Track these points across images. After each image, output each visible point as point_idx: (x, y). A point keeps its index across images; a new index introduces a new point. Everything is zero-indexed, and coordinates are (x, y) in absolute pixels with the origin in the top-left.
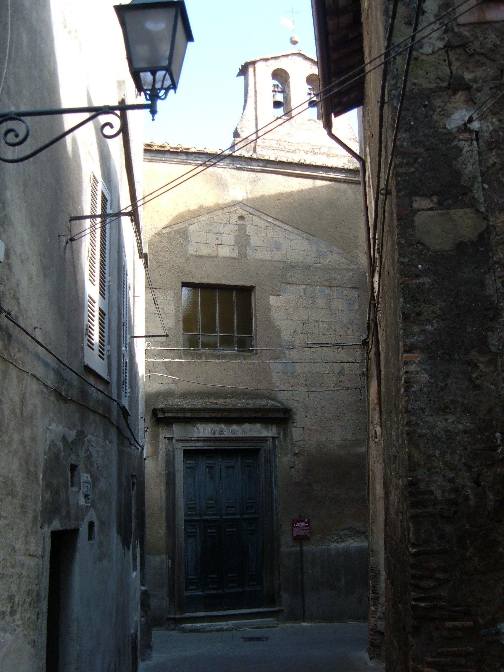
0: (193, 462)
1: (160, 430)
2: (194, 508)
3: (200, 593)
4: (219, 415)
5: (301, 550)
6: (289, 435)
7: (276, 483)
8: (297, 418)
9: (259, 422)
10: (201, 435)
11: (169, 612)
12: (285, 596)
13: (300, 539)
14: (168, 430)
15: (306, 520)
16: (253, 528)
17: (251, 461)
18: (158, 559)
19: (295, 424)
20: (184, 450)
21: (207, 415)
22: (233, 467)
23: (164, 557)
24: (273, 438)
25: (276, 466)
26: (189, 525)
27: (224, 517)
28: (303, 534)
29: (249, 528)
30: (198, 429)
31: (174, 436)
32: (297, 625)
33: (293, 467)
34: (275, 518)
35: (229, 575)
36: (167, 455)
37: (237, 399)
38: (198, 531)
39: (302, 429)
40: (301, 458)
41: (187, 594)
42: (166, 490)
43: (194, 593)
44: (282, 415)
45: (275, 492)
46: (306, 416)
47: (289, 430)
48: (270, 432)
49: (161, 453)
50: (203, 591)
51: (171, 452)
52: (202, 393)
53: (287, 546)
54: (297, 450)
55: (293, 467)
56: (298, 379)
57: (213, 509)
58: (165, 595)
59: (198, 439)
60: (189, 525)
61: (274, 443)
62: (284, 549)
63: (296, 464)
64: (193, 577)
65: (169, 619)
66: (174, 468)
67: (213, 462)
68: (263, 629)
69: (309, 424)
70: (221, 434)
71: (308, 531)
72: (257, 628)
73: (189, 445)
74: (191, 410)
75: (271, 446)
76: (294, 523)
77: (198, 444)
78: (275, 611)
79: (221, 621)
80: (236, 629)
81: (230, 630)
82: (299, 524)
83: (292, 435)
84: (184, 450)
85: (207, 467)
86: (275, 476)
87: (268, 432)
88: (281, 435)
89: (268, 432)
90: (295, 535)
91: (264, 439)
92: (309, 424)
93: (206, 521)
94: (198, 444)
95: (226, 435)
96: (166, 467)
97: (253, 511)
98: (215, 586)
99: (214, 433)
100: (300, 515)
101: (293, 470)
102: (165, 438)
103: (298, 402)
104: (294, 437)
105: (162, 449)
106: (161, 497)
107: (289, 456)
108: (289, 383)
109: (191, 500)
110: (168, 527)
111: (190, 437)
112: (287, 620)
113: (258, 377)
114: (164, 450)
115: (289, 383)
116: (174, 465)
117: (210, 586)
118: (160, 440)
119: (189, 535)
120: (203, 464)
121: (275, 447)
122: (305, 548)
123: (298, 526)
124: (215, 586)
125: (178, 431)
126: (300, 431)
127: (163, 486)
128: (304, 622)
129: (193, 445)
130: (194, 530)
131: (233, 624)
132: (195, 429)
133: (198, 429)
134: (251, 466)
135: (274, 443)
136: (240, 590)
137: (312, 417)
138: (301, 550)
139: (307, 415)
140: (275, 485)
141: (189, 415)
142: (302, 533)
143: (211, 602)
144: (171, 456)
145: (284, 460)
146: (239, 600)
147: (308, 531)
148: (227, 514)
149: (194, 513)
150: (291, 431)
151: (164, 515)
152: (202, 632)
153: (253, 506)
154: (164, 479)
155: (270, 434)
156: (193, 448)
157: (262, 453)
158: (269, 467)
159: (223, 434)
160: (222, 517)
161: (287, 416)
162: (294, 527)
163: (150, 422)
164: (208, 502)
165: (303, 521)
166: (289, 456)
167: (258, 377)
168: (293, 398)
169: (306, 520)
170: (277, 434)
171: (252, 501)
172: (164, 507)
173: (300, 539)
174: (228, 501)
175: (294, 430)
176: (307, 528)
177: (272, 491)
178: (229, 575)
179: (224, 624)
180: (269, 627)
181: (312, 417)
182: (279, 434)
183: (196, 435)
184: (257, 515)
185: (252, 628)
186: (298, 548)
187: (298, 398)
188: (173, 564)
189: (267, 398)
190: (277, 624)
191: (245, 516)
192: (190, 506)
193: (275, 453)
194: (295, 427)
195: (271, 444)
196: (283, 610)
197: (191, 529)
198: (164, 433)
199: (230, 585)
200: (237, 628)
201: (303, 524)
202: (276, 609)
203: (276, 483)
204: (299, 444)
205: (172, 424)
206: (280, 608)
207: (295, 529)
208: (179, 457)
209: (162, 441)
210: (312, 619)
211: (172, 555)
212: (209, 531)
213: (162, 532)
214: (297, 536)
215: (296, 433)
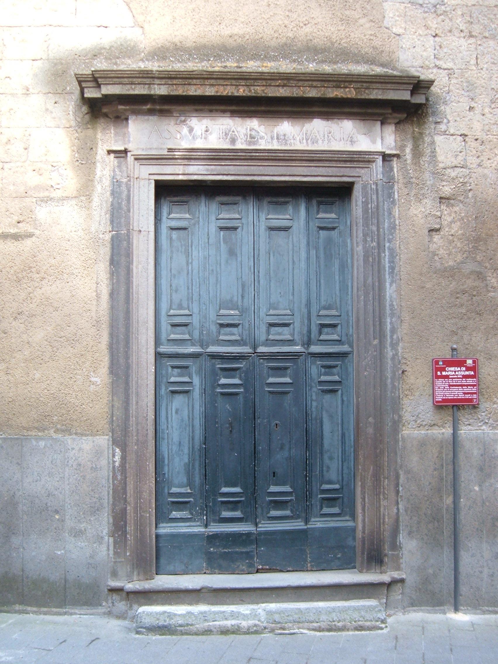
0: (187, 216)
1: (99, 135)
2: (186, 325)
3: (196, 530)
4: (241, 91)
5: (455, 435)
6: (428, 151)
7: (392, 268)
8: (448, 110)
9: (349, 115)
10: (199, 144)
11: (114, 574)
12: (410, 547)
13: (453, 408)
14: (116, 134)
15: (469, 362)
16: (336, 378)
17: (333, 216)
18: (87, 444)
19: (443, 127)
20: (156, 182)
21: (210, 91)
22: (286, 229)
23: (103, 441)
24: (386, 157)
25: (393, 227)
26: (173, 367)
27: (261, 349)
28: (461, 396)
29: (323, 378)
30: (191, 130)
31: (130, 147)
32: (439, 617)
33: (437, 230)
34: (389, 353)
35: (273, 489)
36: (113, 193)
37: (294, 61)
38: (196, 381)
39: (461, 138)
40: (457, 209)
41: (165, 529)
42: (111, 278)
43: (183, 529)
44: (405, 96)
45: (390, 291)
46: (471, 109)
47: (427, 139)
48: (379, 141)
49: (99, 188)
50: (206, 526)
51: (124, 188)
52: (205, 47)
53: (417, 422)
54: (447, 190)
55: (437, 230)
56: (451, 20)
57: (234, 330)
58: (105, 531)
59: (191, 156)
60: (173, 367)
61: (388, 171)
62: (410, 432)
63: (444, 223)
64: (182, 490)
65: (113, 590)
66: (128, 224)
67: (237, 216)
68: (344, 633)
69: (477, 126)
70: (250, 143)
71: (474, 390)
72: (329, 630)
73: (169, 169)
74: (169, 77)
75: (380, 176)
76: (438, 368)
77: (192, 169)
78: (381, 584)
79: (242, 602)
80: (272, 631)
81: (256, 632)
82: (450, 371)
83: (434, 152)
84: (156, 182)
85: (221, 228)
86: (392, 251)
87: (374, 142)
88: (408, 150)
89: (374, 142)
90: (439, 399)
91: (361, 159)
92: (477, 126)
93: (214, 356)
94: (192, 169)
95: (262, 145)
96: (112, 222)
97: (335, 337)
98: (238, 514)
99: (233, 141)
100: (453, 350)
101: (436, 238)
102: (109, 152)
103: (450, 72)
104: (441, 158)
105: (101, 181)
106: (98, 296)
107: (428, 203)
108: (427, 27)
109: (180, 307)
110: (113, 369)
111: (170, 150)
112: (414, 604)
113: (347, 13)
114: (107, 182)
115: (427, 27)
116: (128, 218)
117: (226, 514)
118: (98, 157)
119: (166, 390)
120: (207, 217)
121: (390, 182)
122: (464, 431)
123: (447, 377)
124: (238, 514)
125: (140, 133)
126: (457, 143)
127: (102, 269)
128: (456, 610)
129: (179, 169)
130: (186, 379)
131: (270, 613)
132: (185, 130)
133: (191, 130)
134: (334, 229)
135: (388, 171)
136: (298, 525)
137: (487, 110)
138: (455, 435)
139: (473, 104)
140: (392, 273)
141: (161, 90)
142: (458, 393)
143: (225, 553)
144: (124, 196)
145: (413, 213)
146: (291, 551)
147: (474, 390)
148: (268, 342)
149: (187, 337)
150: (433, 143)
151: (105, 339)
152: (183, 634)
153: (334, 326)
154: (105, 252)
155: (378, 147)
156: (181, 178)
157: (357, 193)
158: (374, 228)
159: (254, 143)
160: (255, 348)
161: (419, 99)
162: (438, 377)
163: (75, 114)
164: (223, 312)
165: (460, 363)
166: (428, 203)
167: (347, 13)
168: (438, 63)
169: (469, 362)
170: (396, 148)
171: (334, 312)
172: (105, 319)
173: (453, 408)
174: (272, 312)
175: (439, 139)
176: (470, 381)
177: (381, 288)
178: (273, 489)
179: (246, 613)
180: (361, 628)
181: (487, 110)
182: (402, 148)
183: (185, 145)
184: (345, 348)
185: (314, 630)
186: (448, 431)
187: (450, 65)
188: (123, 458)
189: (372, 61)
190: (383, 622)
191: (315, 349)
192: (177, 320)
193: (390, 195)
194: (444, 133)
195: (380, 169)
196: (402, 581)
197: (180, 375)
198: (107, 138)
199: (274, 513)
200: (277, 627)
201: (462, 371)
202: (386, 578)
203: (392, 268)
204: (453, 174)
205: (127, 119)
206: (396, 575)
207: (439, 382)
208: (145, 197)
209: (104, 161)
210: (477, 604)
211: (120, 441)
212: (223, 381)
213: (98, 380)
214: (444, 401)
215: (445, 145)
